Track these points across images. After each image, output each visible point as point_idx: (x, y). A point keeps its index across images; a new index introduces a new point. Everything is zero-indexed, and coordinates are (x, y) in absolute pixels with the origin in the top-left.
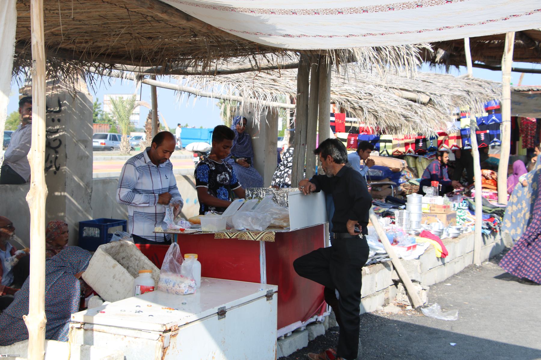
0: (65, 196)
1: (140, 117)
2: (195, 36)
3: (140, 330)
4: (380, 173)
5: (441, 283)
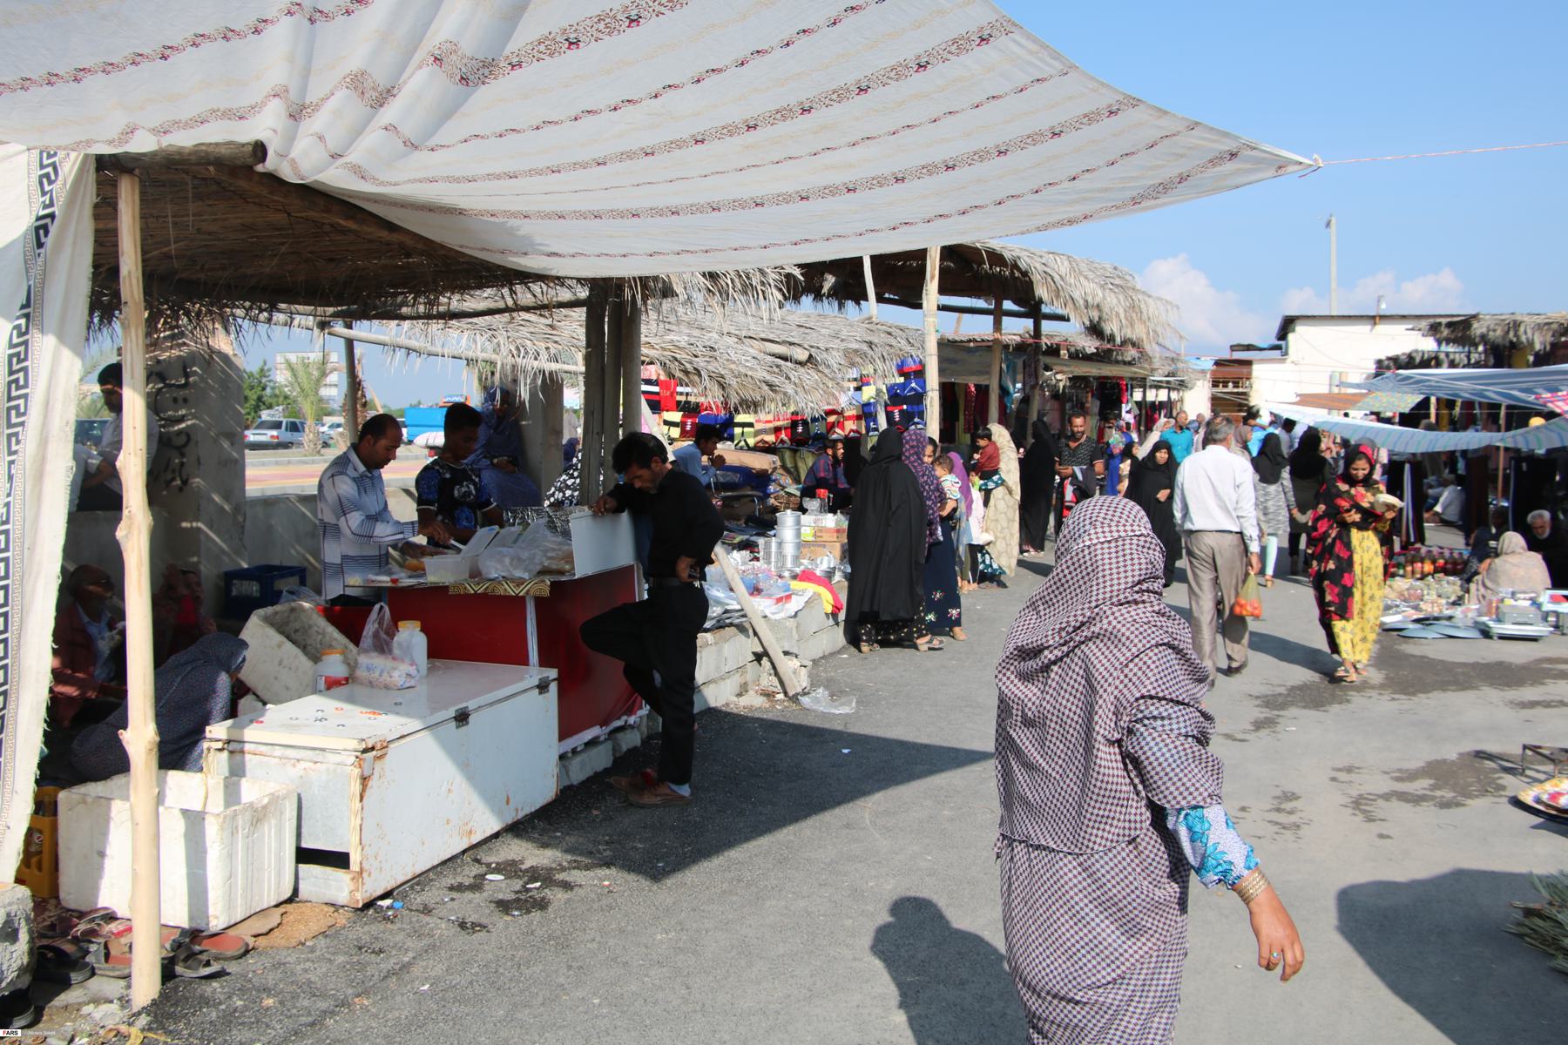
0: (199, 529)
1: (334, 389)
2: (408, 255)
3: (323, 750)
4: (736, 478)
5: (832, 654)
